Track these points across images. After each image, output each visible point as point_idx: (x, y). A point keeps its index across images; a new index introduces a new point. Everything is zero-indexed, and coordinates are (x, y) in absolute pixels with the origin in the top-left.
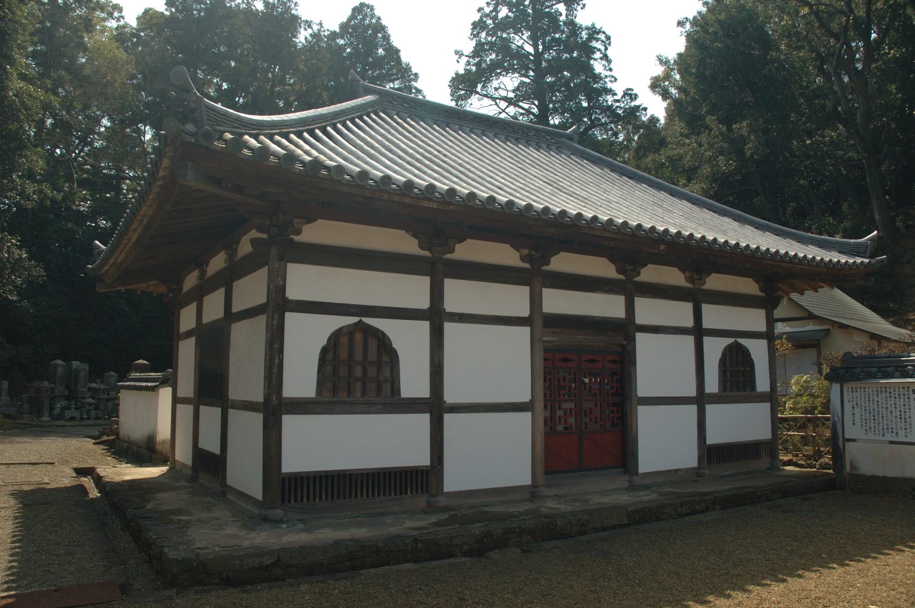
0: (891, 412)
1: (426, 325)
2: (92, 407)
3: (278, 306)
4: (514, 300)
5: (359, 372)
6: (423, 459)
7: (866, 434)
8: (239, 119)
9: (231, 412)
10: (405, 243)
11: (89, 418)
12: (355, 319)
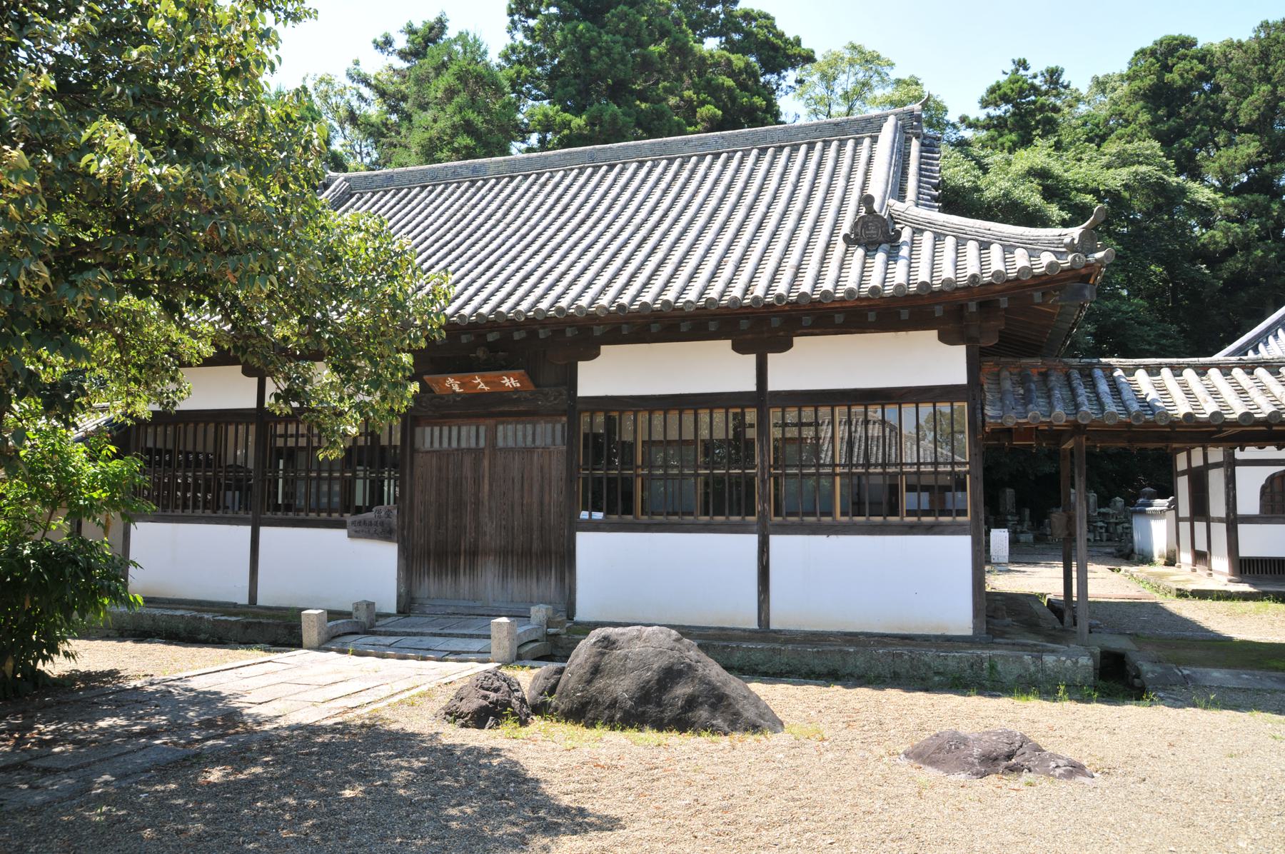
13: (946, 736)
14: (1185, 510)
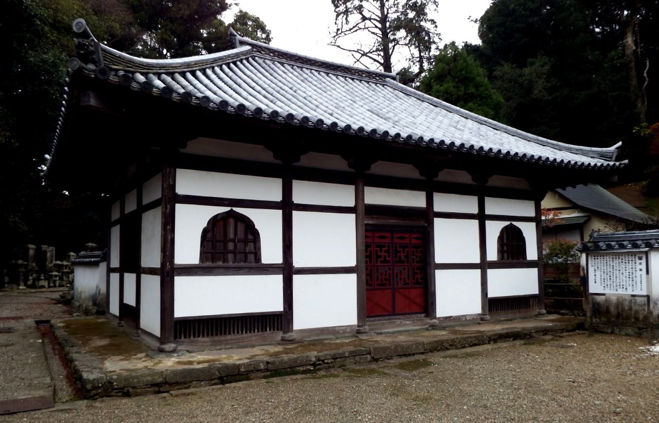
0: (623, 274)
1: (279, 213)
2: (58, 278)
3: (171, 200)
4: (345, 195)
5: (230, 246)
6: (277, 306)
7: (604, 289)
8: (131, 61)
9: (143, 276)
10: (266, 156)
11: (55, 286)
12: (227, 209)
13: (156, 371)
14: (115, 262)
